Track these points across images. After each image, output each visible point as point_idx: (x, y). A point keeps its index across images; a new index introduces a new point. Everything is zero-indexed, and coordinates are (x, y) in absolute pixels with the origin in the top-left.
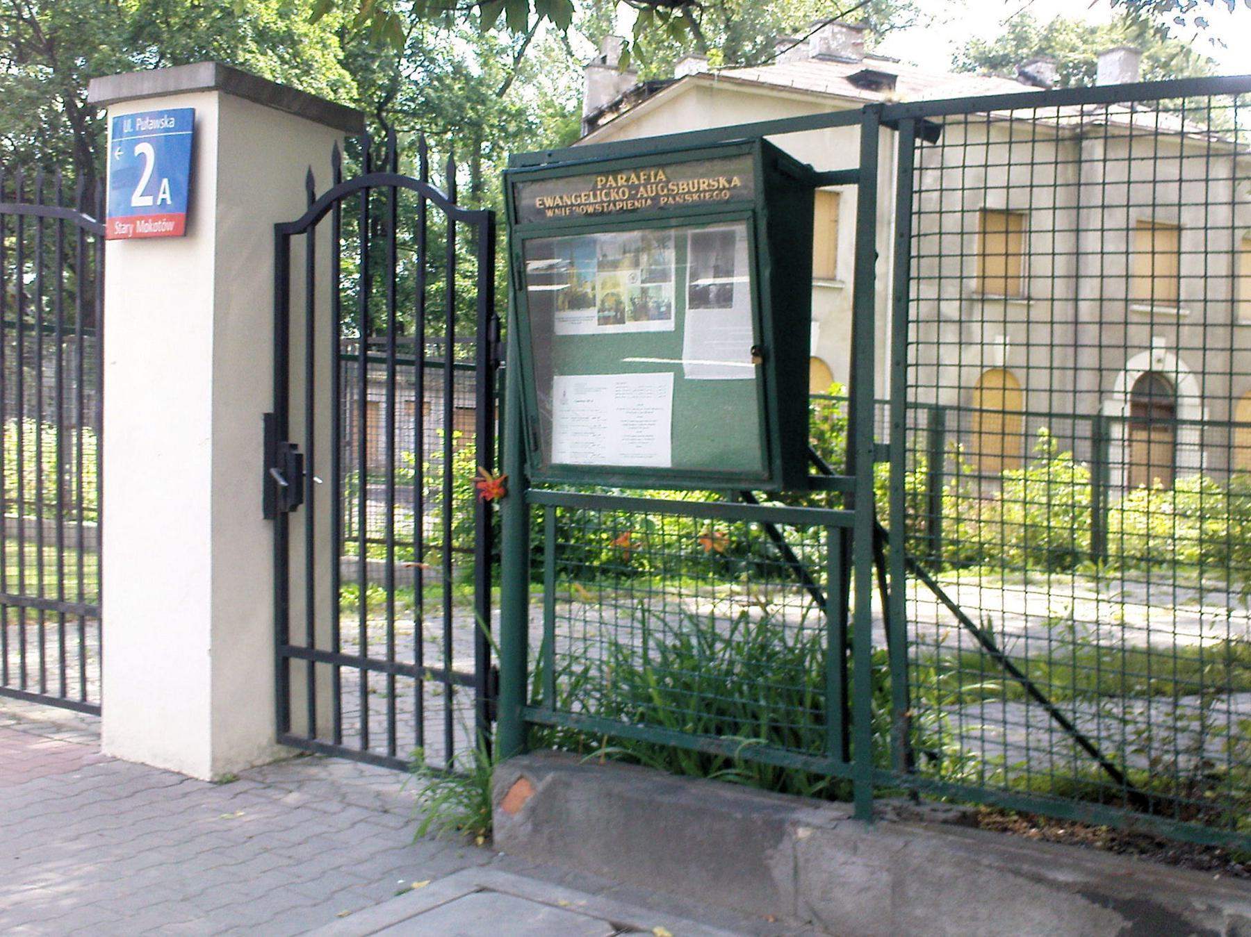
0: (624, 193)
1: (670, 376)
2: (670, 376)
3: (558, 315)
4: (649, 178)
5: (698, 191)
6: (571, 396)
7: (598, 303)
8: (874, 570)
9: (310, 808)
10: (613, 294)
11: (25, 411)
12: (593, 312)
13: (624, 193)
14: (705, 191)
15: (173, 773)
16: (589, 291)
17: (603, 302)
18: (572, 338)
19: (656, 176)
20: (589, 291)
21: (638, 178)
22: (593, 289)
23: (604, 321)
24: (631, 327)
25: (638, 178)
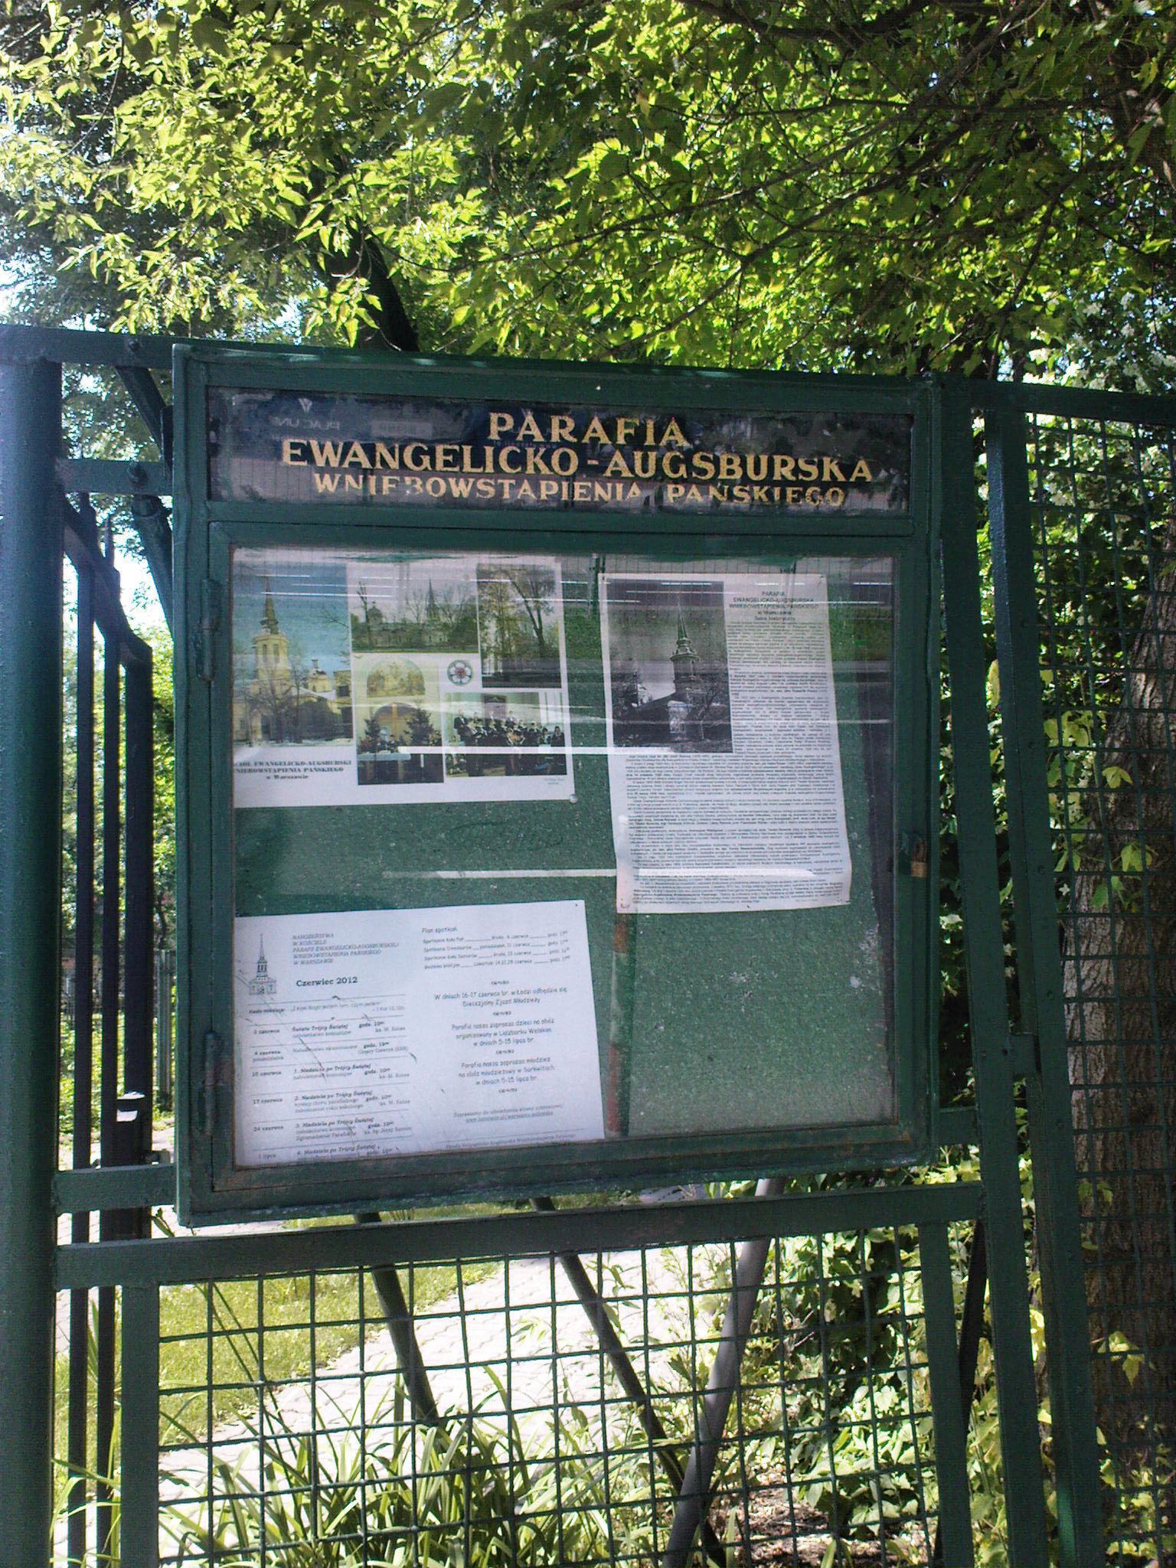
0: (565, 461)
1: (572, 914)
2: (572, 914)
3: (243, 755)
4: (641, 431)
5: (769, 481)
6: (284, 970)
7: (359, 727)
8: (987, 1315)
9: (557, 1440)
10: (403, 710)
11: (869, 684)
12: (345, 751)
13: (565, 461)
14: (784, 483)
15: (871, 1123)
16: (331, 696)
17: (373, 728)
18: (280, 816)
19: (659, 434)
20: (331, 696)
21: (610, 429)
22: (344, 691)
23: (375, 773)
24: (455, 790)
25: (610, 429)
